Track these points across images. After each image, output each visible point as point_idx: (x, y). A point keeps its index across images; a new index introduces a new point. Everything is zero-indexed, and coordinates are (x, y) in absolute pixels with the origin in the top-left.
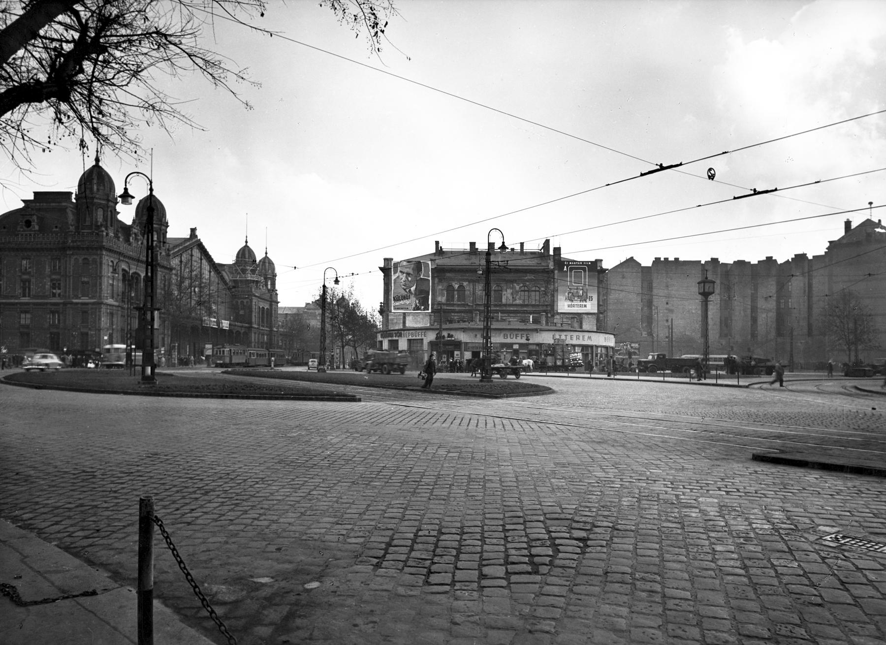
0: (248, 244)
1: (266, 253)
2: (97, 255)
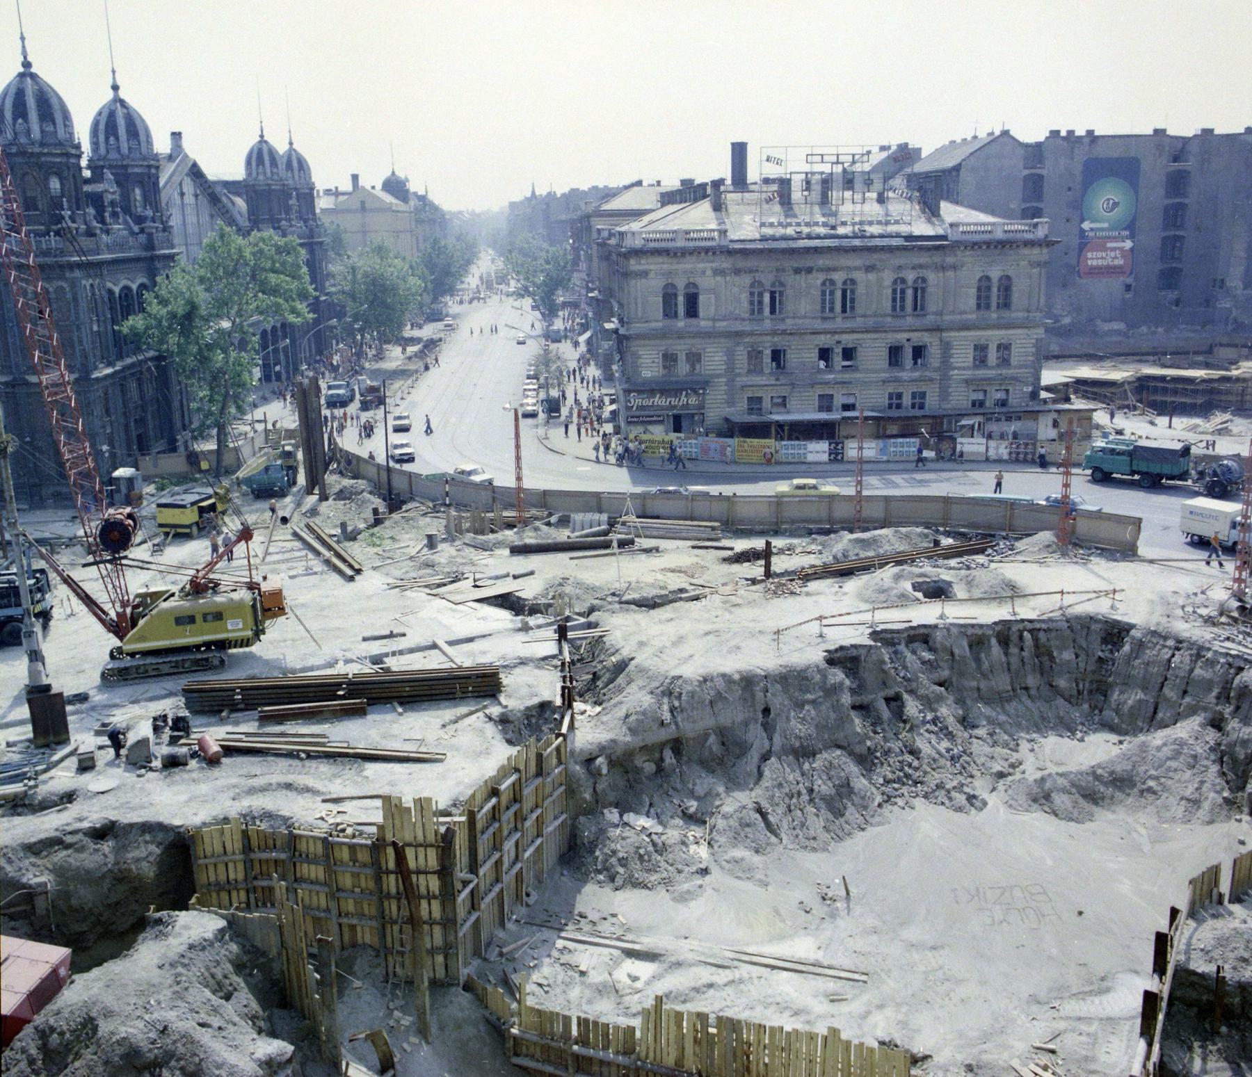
0: (123, 94)
1: (115, 88)
2: (66, 279)
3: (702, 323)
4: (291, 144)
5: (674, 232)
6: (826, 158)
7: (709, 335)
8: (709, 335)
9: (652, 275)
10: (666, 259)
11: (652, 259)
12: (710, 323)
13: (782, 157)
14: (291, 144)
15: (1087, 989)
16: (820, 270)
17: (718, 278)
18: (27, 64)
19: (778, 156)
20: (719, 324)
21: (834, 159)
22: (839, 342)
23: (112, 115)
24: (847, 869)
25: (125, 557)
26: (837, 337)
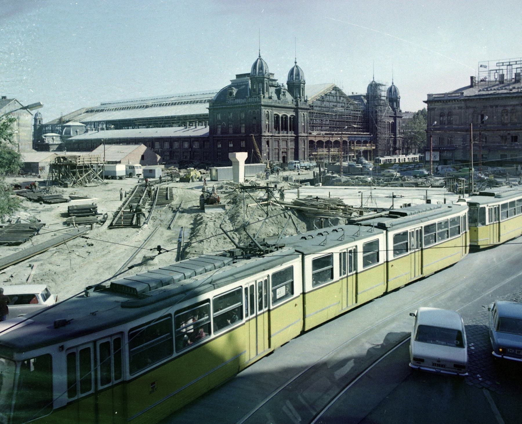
1: (296, 63)
3: (454, 126)
4: (393, 83)
5: (444, 94)
6: (504, 64)
7: (456, 130)
8: (456, 130)
9: (436, 110)
10: (441, 104)
11: (437, 104)
12: (457, 127)
13: (487, 65)
14: (393, 83)
15: (316, 174)
16: (501, 106)
17: (460, 110)
18: (260, 56)
19: (485, 65)
20: (460, 127)
21: (508, 64)
22: (509, 134)
23: (293, 69)
24: (310, 175)
25: (286, 212)
26: (508, 132)
